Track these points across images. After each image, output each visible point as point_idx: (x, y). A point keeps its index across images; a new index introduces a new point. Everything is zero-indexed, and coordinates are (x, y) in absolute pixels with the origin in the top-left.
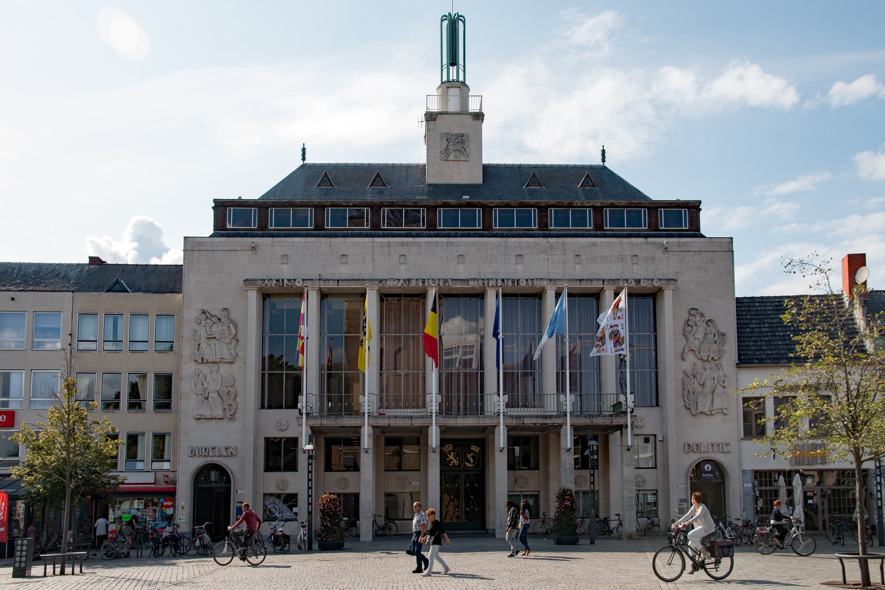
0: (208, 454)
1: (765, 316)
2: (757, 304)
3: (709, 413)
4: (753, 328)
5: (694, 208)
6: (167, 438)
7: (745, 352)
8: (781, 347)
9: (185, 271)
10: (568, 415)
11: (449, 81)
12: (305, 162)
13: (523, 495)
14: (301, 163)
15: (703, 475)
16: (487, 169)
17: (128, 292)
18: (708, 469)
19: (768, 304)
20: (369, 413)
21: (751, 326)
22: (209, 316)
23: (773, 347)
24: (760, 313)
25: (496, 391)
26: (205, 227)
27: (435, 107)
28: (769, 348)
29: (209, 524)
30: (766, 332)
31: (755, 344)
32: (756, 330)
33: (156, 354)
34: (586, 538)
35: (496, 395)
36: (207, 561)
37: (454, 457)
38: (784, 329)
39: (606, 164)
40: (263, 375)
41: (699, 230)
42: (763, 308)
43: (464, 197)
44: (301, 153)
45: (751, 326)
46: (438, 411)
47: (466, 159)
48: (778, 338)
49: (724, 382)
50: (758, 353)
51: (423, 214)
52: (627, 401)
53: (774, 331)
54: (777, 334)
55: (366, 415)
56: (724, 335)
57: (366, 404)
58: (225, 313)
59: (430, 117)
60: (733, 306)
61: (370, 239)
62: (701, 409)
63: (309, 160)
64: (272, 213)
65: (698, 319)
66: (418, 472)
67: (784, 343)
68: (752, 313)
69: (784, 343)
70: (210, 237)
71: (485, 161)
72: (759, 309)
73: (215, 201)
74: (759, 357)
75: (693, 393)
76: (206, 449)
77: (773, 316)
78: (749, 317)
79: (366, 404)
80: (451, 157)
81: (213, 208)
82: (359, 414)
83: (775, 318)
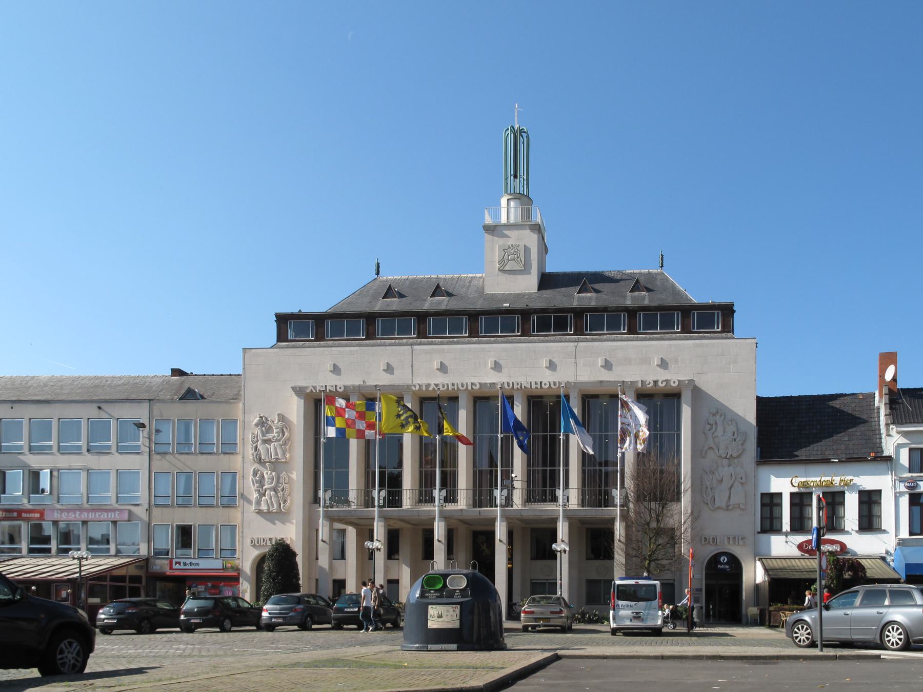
0: (266, 543)
6: (759, 531)
9: (891, 387)
11: (519, 193)
13: (549, 583)
15: (719, 566)
18: (723, 561)
29: (804, 603)
36: (517, 635)
49: (742, 478)
62: (717, 504)
66: (398, 561)
75: (711, 489)
76: (264, 540)
82: (496, 506)
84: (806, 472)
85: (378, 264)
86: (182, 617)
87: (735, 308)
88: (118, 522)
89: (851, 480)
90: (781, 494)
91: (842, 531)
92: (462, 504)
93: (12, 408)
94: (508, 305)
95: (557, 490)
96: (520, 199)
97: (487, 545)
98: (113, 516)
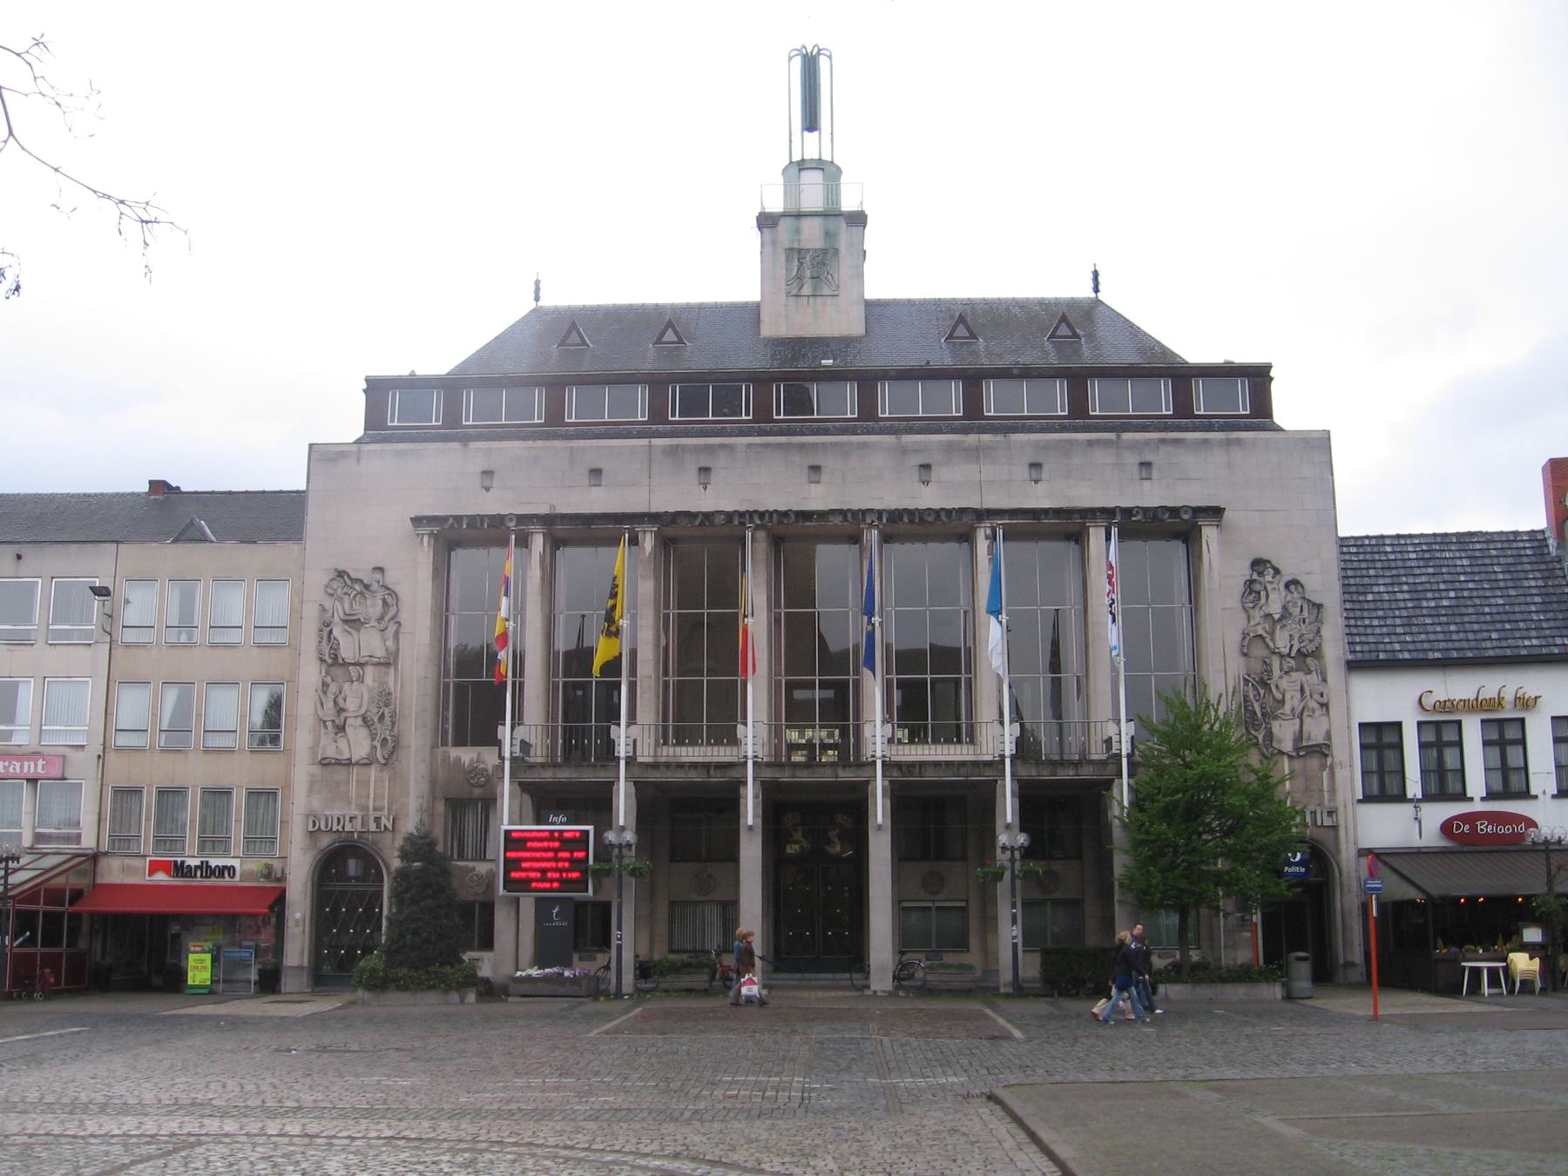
0: (343, 827)
1: (1402, 572)
2: (1388, 549)
3: (1294, 754)
4: (1379, 593)
5: (1258, 377)
7: (1363, 639)
8: (1430, 628)
9: (312, 501)
10: (1008, 761)
12: (540, 304)
14: (533, 305)
15: (1286, 869)
16: (871, 306)
17: (212, 542)
19: (1410, 549)
20: (756, 757)
21: (1376, 589)
22: (349, 582)
23: (1415, 629)
24: (1393, 564)
25: (996, 716)
26: (348, 424)
27: (776, 205)
28: (1407, 629)
30: (1404, 600)
31: (1382, 623)
32: (1386, 597)
33: (255, 651)
34: (356, 870)
35: (996, 724)
37: (804, 837)
38: (1437, 595)
39: (1101, 296)
40: (969, 671)
41: (1269, 415)
42: (1399, 556)
43: (823, 362)
44: (533, 287)
45: (1376, 589)
46: (1014, 752)
47: (834, 293)
48: (1425, 612)
50: (1387, 640)
51: (746, 392)
52: (1120, 734)
53: (1418, 599)
54: (1425, 604)
55: (622, 763)
56: (1319, 606)
57: (750, 740)
58: (378, 576)
59: (766, 221)
60: (1331, 554)
61: (645, 442)
63: (550, 300)
64: (470, 399)
65: (1269, 578)
67: (1436, 620)
68: (1379, 565)
69: (1436, 620)
70: (356, 442)
71: (870, 294)
72: (1392, 557)
73: (368, 380)
74: (1389, 647)
77: (1417, 571)
78: (1372, 572)
79: (750, 740)
80: (807, 290)
81: (365, 391)
83: (1421, 575)
84: (1445, 682)
85: (537, 283)
86: (1294, 830)
87: (1272, 374)
88: (39, 782)
89: (1536, 698)
90: (1398, 726)
91: (1525, 794)
92: (646, 753)
93: (19, 557)
94: (830, 362)
95: (740, 727)
96: (823, 169)
97: (803, 832)
98: (32, 770)
